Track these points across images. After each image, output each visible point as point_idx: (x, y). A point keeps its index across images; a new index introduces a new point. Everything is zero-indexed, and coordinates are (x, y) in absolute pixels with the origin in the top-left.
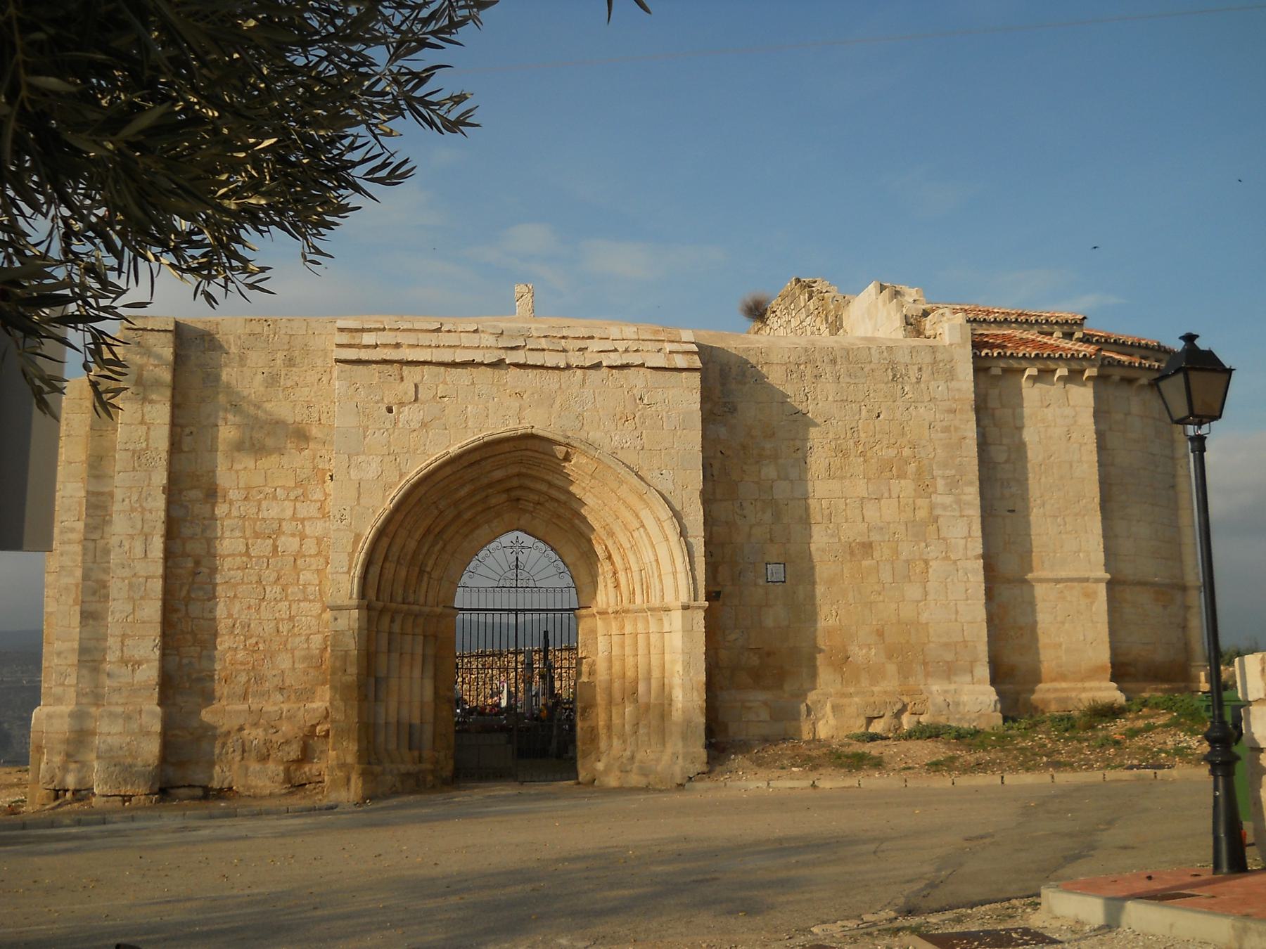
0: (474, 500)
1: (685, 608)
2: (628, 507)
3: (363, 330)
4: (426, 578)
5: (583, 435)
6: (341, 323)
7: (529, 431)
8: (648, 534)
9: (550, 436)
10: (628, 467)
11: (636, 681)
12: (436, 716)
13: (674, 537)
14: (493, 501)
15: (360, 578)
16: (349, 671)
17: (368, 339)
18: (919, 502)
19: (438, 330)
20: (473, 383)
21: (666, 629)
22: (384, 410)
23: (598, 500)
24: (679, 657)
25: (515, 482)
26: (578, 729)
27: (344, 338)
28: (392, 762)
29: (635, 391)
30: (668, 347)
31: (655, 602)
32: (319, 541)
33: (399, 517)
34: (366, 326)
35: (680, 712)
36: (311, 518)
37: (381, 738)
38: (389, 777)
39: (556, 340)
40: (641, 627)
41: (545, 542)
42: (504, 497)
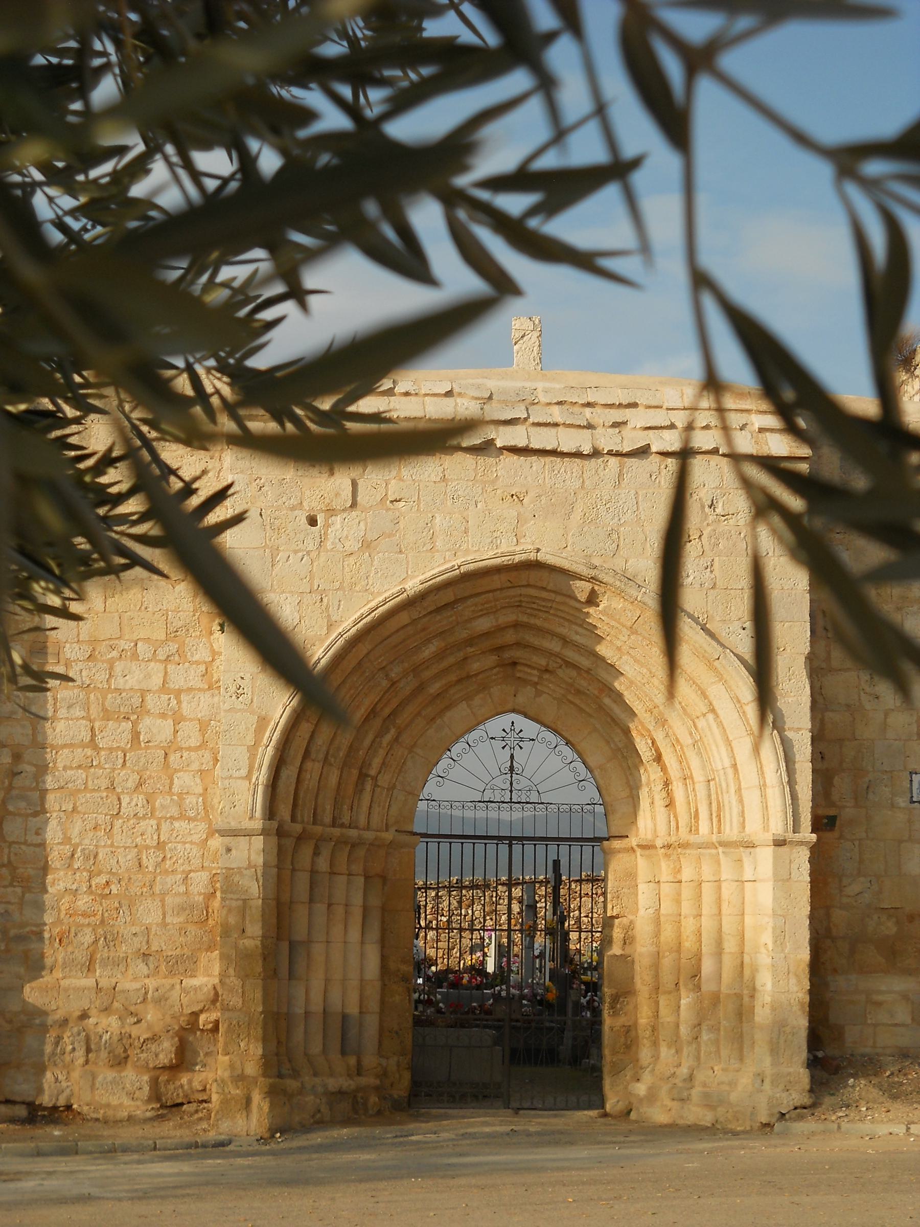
1: (779, 843)
4: (368, 787)
7: (532, 556)
8: (720, 724)
9: (566, 565)
11: (698, 957)
12: (383, 1002)
14: (476, 666)
15: (267, 786)
20: (444, 479)
21: (748, 874)
24: (768, 922)
25: (510, 637)
28: (315, 1075)
31: (731, 832)
35: (767, 1010)
36: (190, 689)
37: (298, 1035)
38: (310, 1099)
39: (577, 409)
40: (707, 872)
41: (556, 731)
42: (492, 659)
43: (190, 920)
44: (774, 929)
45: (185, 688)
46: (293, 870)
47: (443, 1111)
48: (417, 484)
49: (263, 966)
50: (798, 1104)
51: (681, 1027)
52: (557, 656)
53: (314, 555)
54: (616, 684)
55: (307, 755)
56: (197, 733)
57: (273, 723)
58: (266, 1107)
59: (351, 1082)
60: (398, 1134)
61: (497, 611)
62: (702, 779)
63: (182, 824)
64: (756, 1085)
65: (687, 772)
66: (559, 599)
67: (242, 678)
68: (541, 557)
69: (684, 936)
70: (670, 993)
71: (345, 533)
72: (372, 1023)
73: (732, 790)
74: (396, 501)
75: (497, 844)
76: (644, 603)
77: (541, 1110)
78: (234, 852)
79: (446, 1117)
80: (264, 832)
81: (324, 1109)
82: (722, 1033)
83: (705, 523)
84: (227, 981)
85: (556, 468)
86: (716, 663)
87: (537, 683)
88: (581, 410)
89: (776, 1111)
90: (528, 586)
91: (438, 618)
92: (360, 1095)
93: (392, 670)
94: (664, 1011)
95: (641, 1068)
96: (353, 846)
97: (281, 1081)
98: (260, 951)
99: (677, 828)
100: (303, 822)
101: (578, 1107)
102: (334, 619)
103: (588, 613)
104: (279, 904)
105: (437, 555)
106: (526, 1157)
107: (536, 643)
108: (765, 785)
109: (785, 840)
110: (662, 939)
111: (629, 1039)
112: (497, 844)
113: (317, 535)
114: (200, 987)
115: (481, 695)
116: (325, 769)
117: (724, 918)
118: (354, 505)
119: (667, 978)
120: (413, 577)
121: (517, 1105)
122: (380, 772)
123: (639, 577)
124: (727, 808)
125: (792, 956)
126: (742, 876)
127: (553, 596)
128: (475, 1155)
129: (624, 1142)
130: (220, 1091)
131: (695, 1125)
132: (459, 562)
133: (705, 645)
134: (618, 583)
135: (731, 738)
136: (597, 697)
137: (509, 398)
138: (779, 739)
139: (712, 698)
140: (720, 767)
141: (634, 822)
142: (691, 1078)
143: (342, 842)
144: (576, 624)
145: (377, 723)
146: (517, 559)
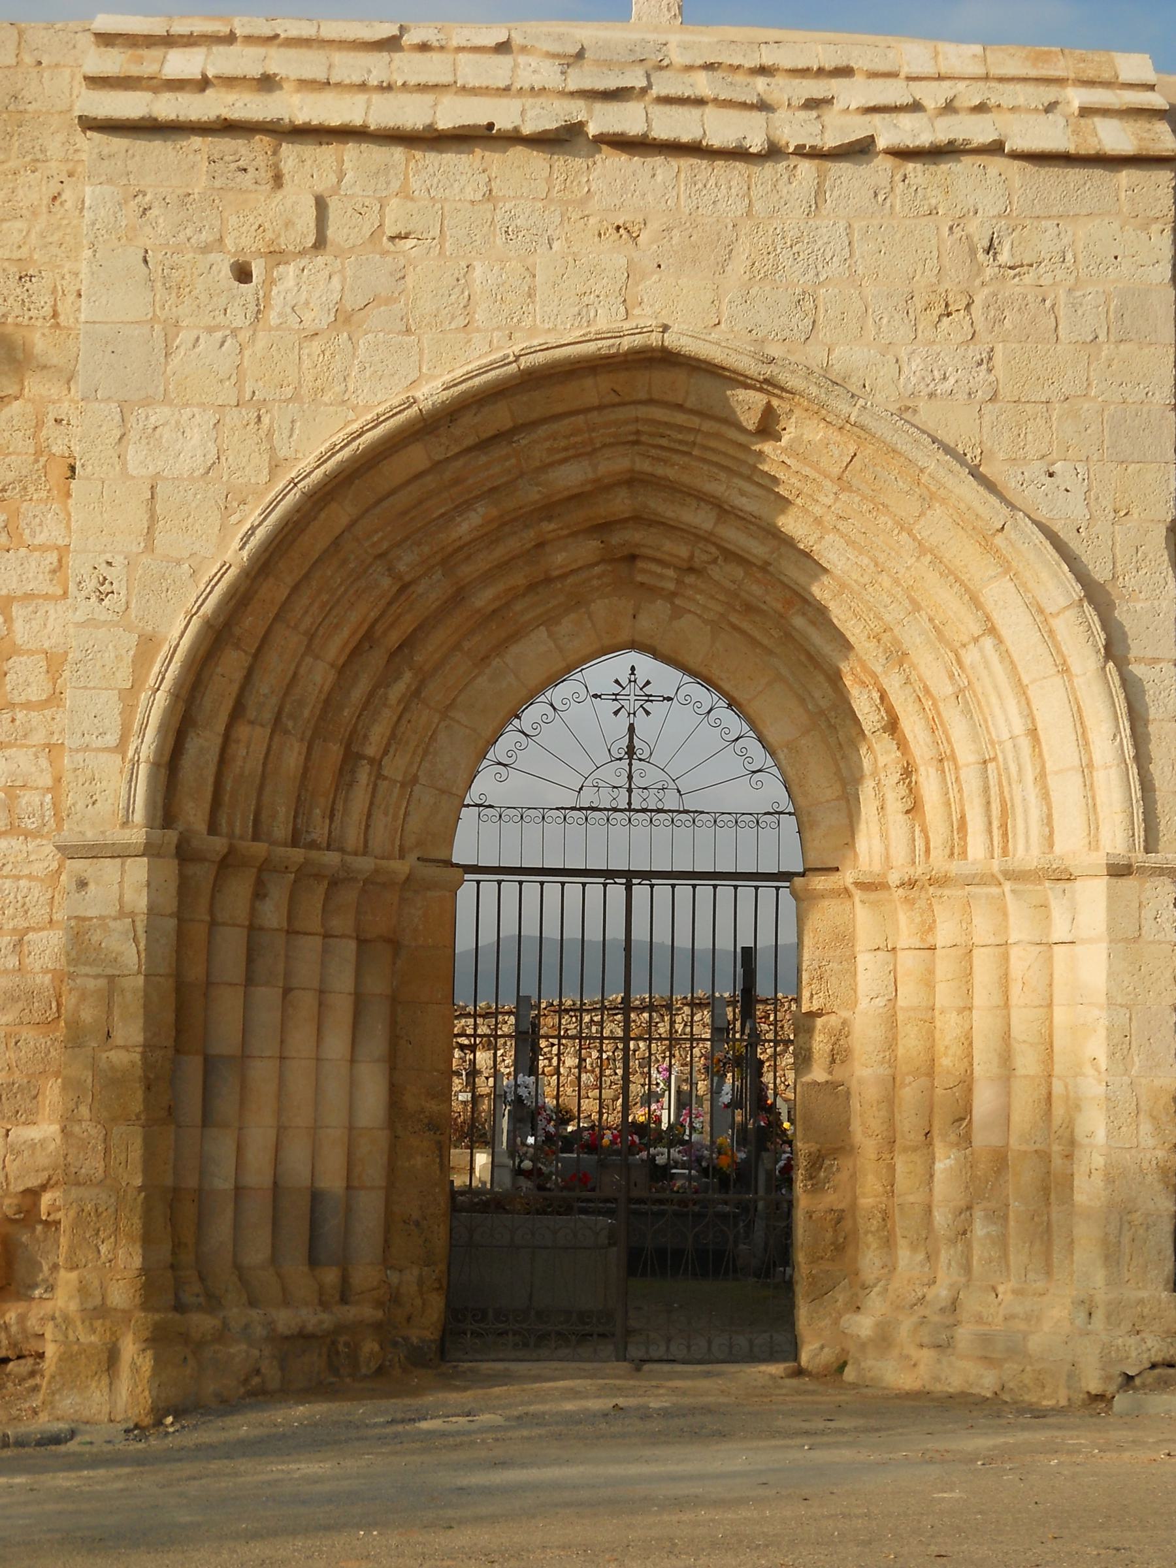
0: (499, 552)
1: (1119, 871)
2: (952, 575)
3: (169, 41)
4: (364, 775)
5: (815, 355)
6: (106, 22)
7: (654, 340)
8: (1006, 656)
9: (716, 355)
10: (948, 450)
11: (967, 1084)
12: (392, 1169)
13: (1085, 660)
14: (559, 559)
15: (156, 765)
16: (119, 1037)
17: (181, 63)
19: (391, 44)
20: (489, 196)
21: (1060, 932)
22: (225, 271)
23: (868, 553)
24: (1098, 1018)
25: (621, 503)
26: (800, 1215)
27: (113, 62)
28: (252, 1303)
29: (973, 226)
30: (1076, 97)
31: (1027, 852)
32: (54, 663)
33: (274, 591)
34: (180, 27)
35: (1098, 1180)
36: (29, 597)
37: (221, 1231)
38: (238, 1349)
39: (740, 78)
40: (982, 928)
41: (708, 682)
42: (588, 549)
43: (26, 1020)
44: (1110, 1031)
45: (19, 593)
46: (213, 923)
47: (500, 1366)
48: (438, 206)
49: (146, 1100)
50: (1158, 1359)
51: (936, 1213)
52: (707, 540)
53: (244, 336)
54: (816, 590)
55: (238, 712)
56: (42, 676)
57: (166, 648)
58: (146, 1364)
59: (325, 1316)
60: (399, 1416)
61: (594, 451)
62: (972, 758)
63: (13, 842)
64: (1078, 1322)
65: (945, 748)
66: (708, 426)
67: (109, 564)
68: (672, 341)
69: (940, 1047)
70: (915, 1149)
71: (304, 296)
72: (370, 1208)
73: (1029, 777)
74: (400, 237)
75: (605, 885)
76: (862, 428)
77: (684, 1362)
78: (92, 887)
79: (506, 1378)
80: (150, 850)
81: (271, 1371)
82: (1012, 1223)
83: (978, 282)
84: (77, 1129)
85: (701, 177)
86: (999, 540)
87: (674, 594)
88: (749, 79)
89: (1116, 1370)
90: (650, 402)
91: (483, 459)
92: (342, 1339)
93: (399, 558)
94: (902, 1181)
95: (864, 1287)
96: (334, 883)
97: (177, 1316)
98: (139, 1072)
99: (927, 851)
100: (231, 836)
101: (753, 1357)
102: (281, 454)
103: (761, 453)
104: (181, 987)
105: (476, 337)
106: (614, 1470)
107: (669, 514)
108: (1090, 765)
109: (1129, 866)
110: (901, 1051)
111: (842, 1236)
112: (605, 885)
113: (251, 299)
114: (43, 1142)
115: (573, 616)
116: (276, 739)
117: (1014, 1013)
118: (320, 243)
119: (908, 1124)
120: (434, 377)
121: (640, 1354)
122: (386, 752)
123: (854, 380)
124: (1019, 811)
125: (1143, 1081)
126: (1048, 935)
127: (695, 422)
128: (523, 1465)
129: (823, 1433)
130: (60, 1337)
131: (963, 1394)
132: (517, 349)
133: (981, 510)
134: (814, 390)
135: (1025, 681)
136: (781, 616)
137: (615, 57)
138: (1117, 679)
139: (990, 607)
140: (1005, 736)
141: (849, 842)
142: (954, 1305)
143: (305, 875)
144: (740, 475)
145: (376, 659)
146: (626, 344)
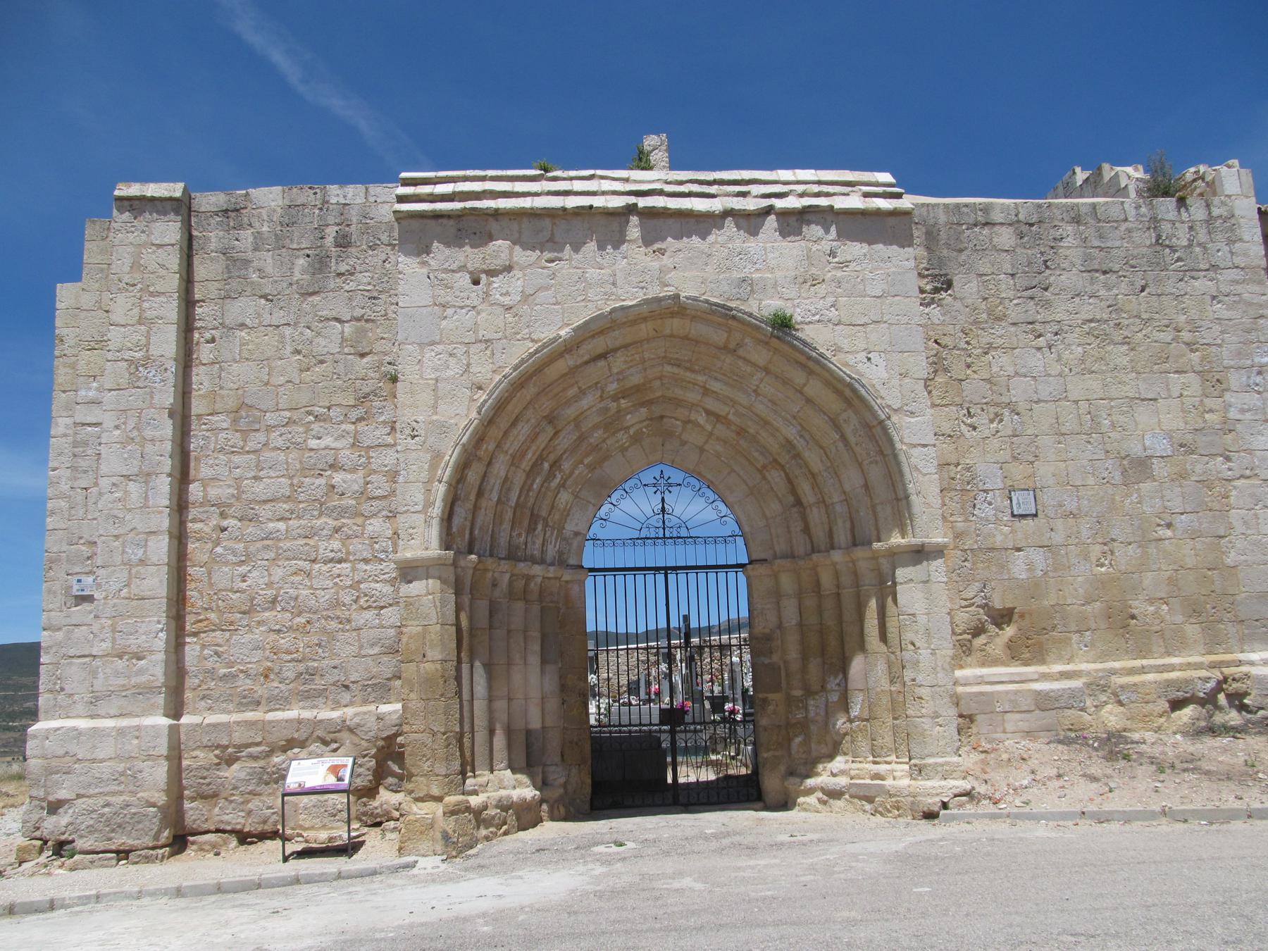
15: (442, 520)
16: (430, 654)
18: (1209, 403)
